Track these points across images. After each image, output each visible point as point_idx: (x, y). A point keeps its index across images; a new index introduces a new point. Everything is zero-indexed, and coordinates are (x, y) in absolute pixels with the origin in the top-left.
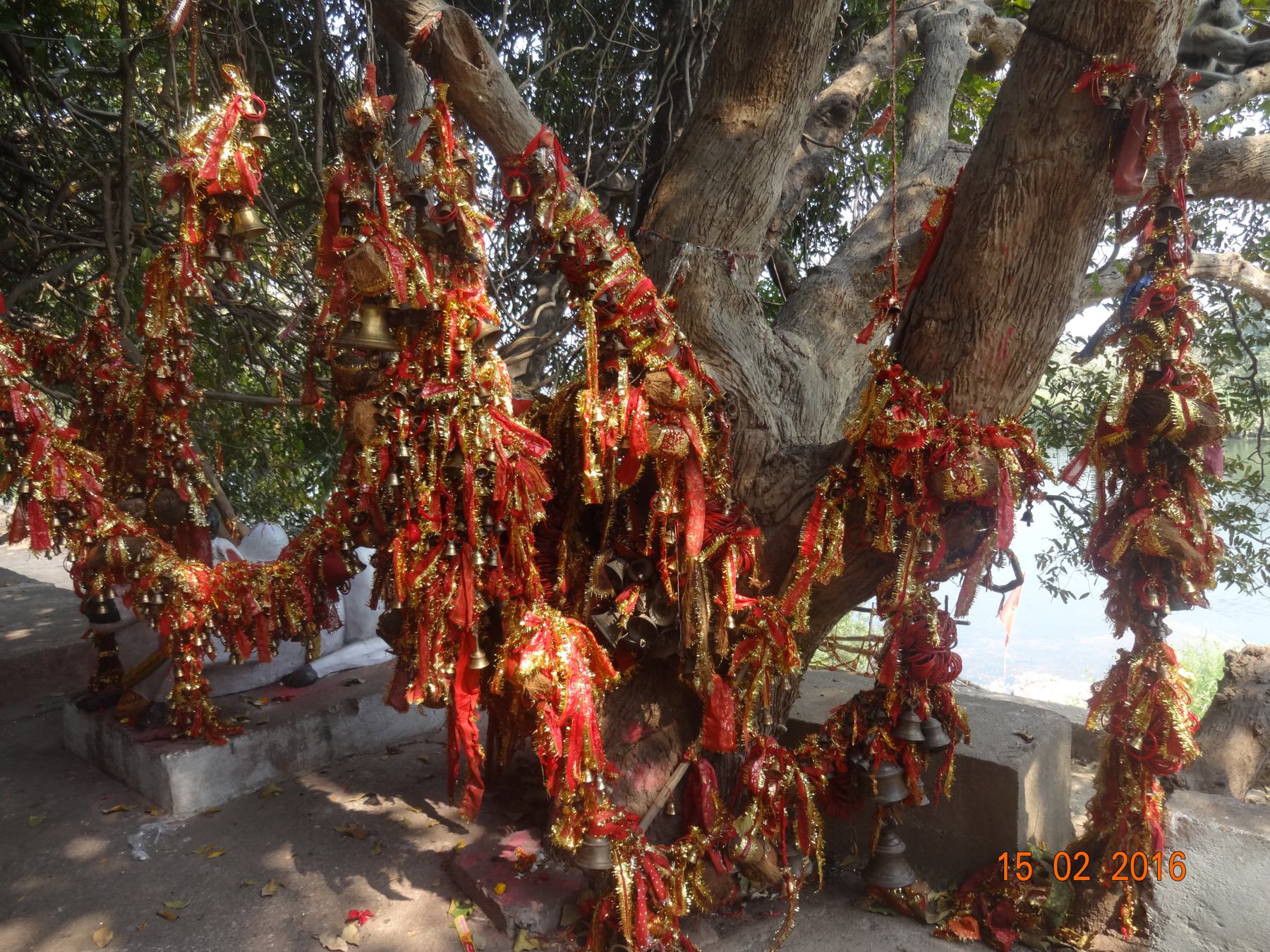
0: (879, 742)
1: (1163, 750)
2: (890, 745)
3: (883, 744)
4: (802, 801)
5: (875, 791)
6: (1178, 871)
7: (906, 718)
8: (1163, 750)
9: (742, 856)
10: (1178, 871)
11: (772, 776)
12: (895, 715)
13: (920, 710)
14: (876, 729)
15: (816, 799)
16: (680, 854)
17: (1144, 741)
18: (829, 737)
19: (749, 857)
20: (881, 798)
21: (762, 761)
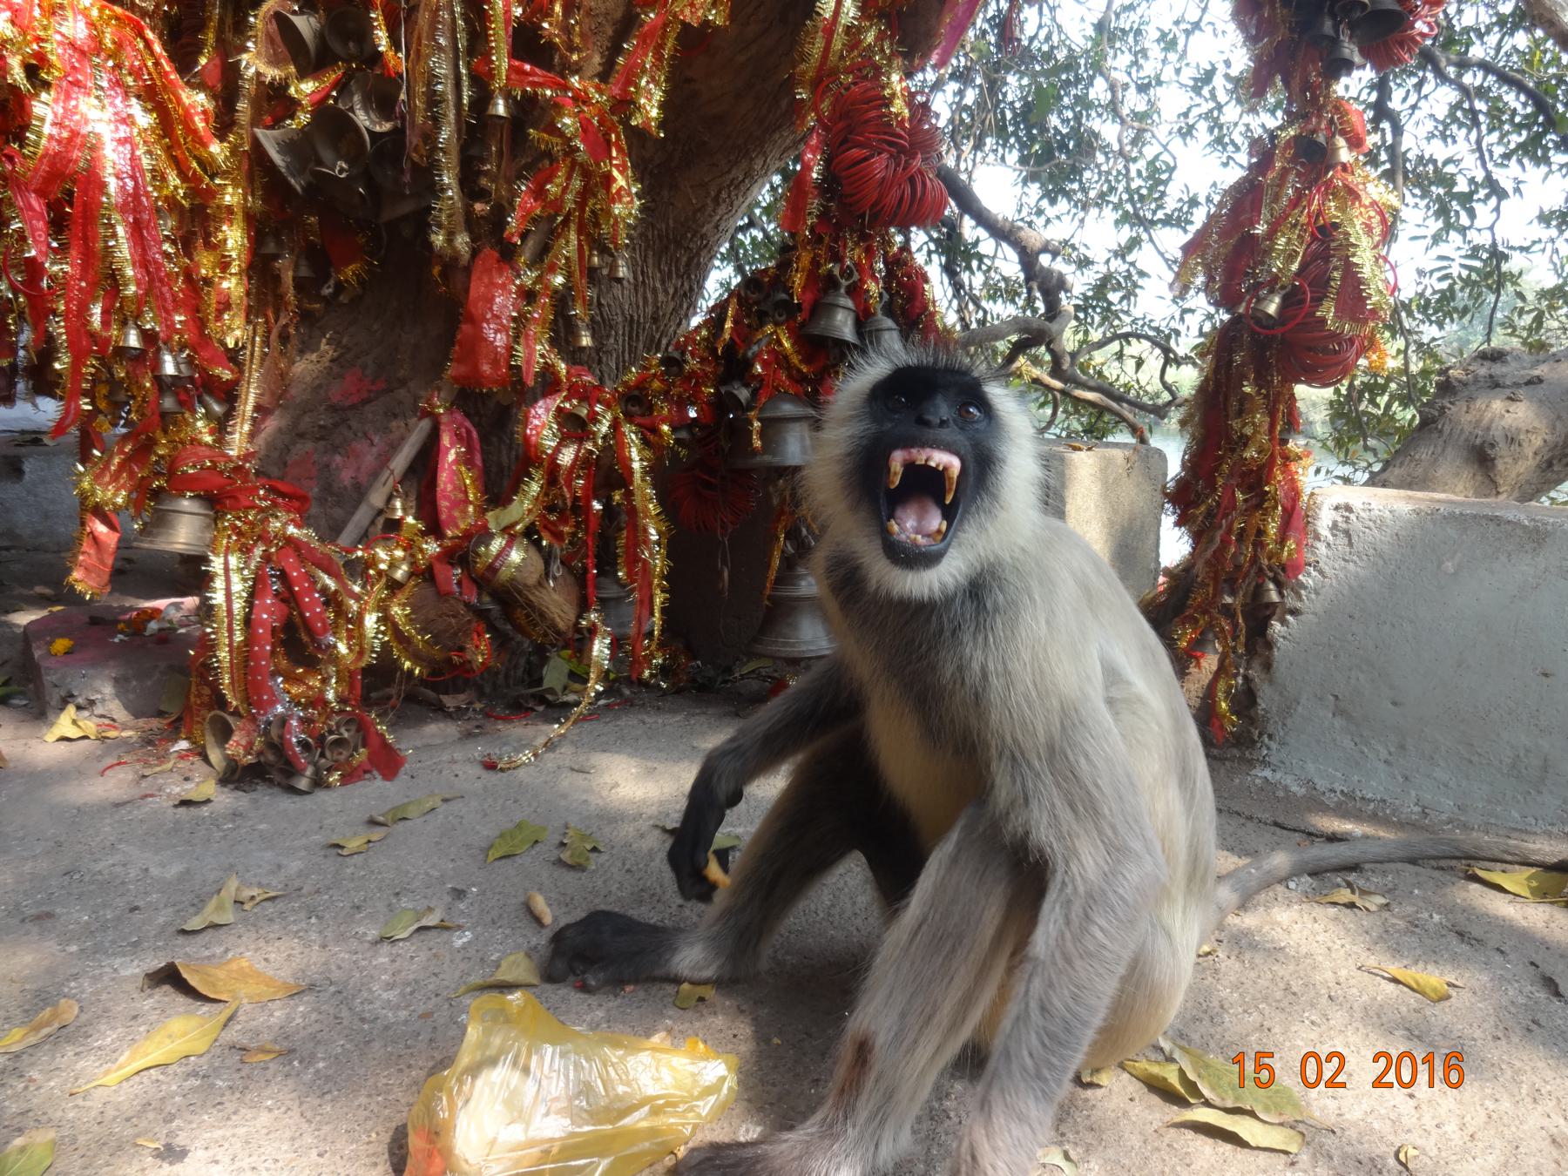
0: (771, 352)
1: (1328, 311)
2: (795, 360)
3: (780, 359)
4: (623, 479)
5: (757, 443)
6: (1454, 1077)
7: (829, 299)
8: (1328, 311)
9: (493, 569)
10: (1454, 1077)
11: (573, 427)
12: (809, 296)
13: (856, 291)
14: (769, 329)
15: (652, 471)
16: (372, 562)
17: (1284, 299)
18: (683, 353)
19: (504, 574)
20: (767, 458)
21: (557, 401)
